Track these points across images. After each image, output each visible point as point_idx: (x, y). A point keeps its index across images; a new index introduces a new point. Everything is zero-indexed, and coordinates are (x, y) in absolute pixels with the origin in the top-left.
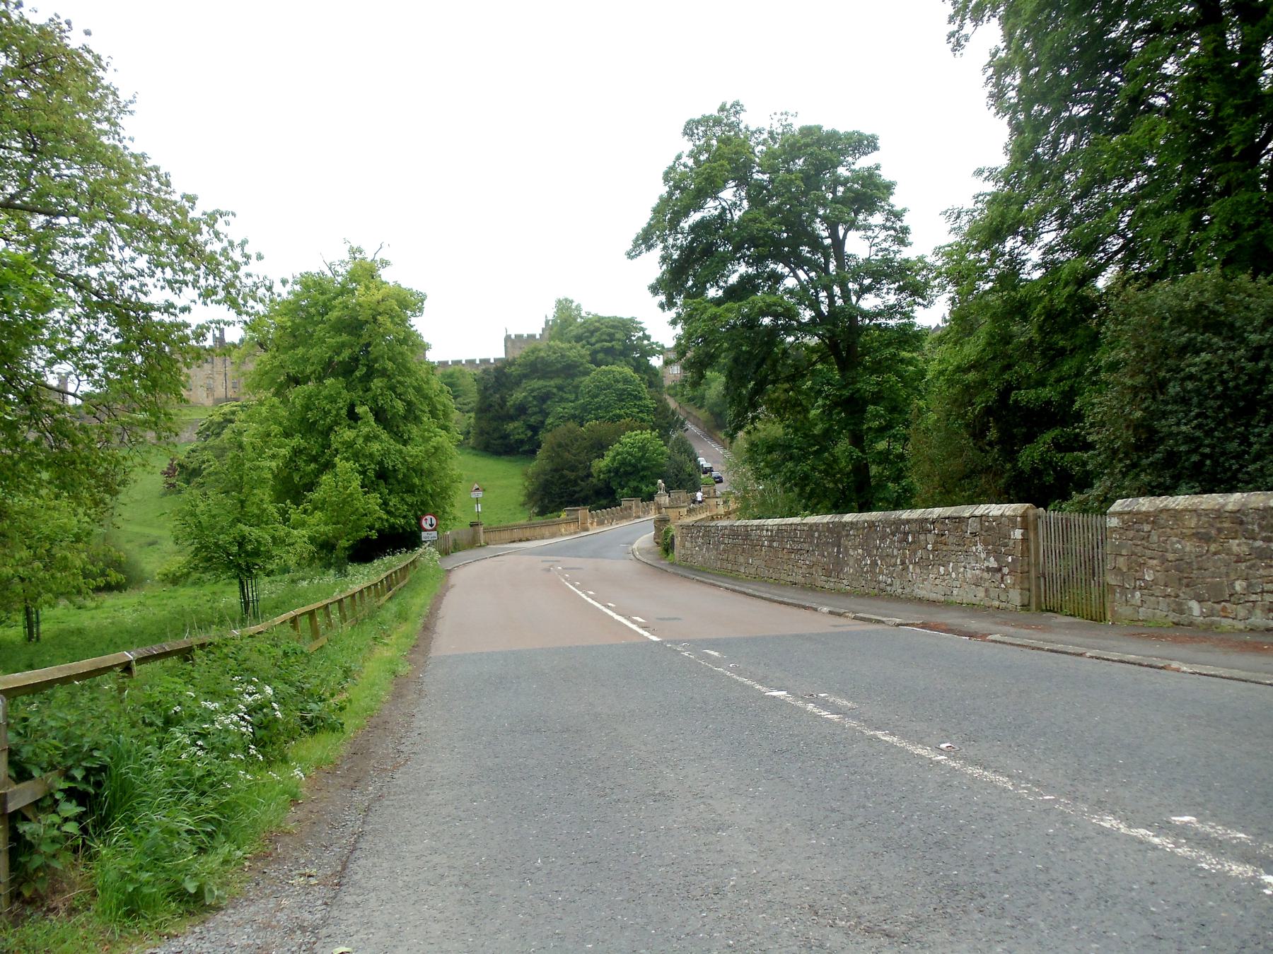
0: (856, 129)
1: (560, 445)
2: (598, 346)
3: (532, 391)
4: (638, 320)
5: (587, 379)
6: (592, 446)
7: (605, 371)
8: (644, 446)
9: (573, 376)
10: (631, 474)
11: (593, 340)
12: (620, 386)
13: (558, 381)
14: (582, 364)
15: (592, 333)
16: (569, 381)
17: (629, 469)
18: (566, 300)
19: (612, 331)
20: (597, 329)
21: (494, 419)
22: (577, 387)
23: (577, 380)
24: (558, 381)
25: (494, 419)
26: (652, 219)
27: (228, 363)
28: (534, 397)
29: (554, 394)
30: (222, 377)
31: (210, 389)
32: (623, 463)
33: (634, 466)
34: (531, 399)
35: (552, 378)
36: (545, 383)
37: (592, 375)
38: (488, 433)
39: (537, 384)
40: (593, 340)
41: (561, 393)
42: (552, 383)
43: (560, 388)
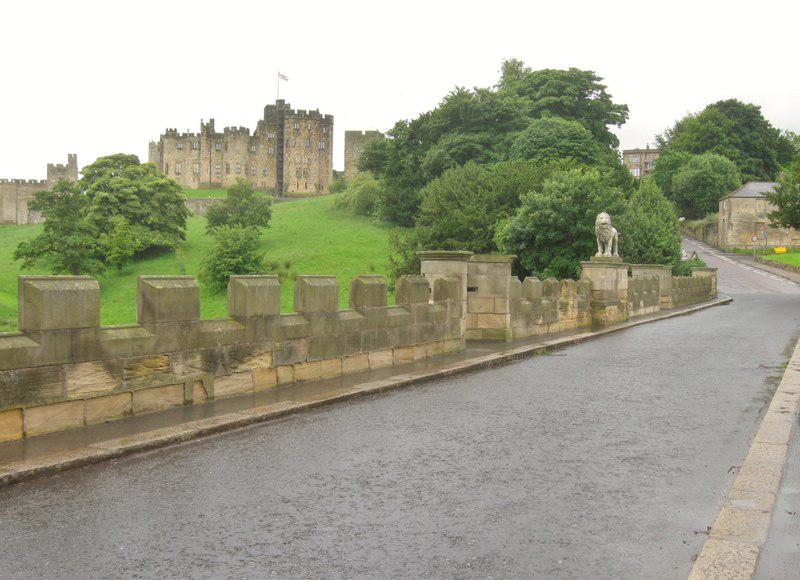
0: (714, 99)
1: (450, 197)
2: (543, 101)
3: (451, 146)
4: (597, 75)
5: (522, 134)
6: (501, 201)
7: (546, 123)
8: (584, 196)
9: (504, 130)
10: (558, 243)
11: (538, 94)
12: (564, 142)
13: (486, 136)
14: (517, 115)
15: (537, 87)
16: (500, 136)
17: (552, 235)
18: (514, 61)
19: (563, 83)
20: (545, 81)
21: (404, 185)
22: (509, 144)
23: (510, 135)
24: (486, 136)
25: (404, 185)
26: (605, 98)
27: (213, 150)
28: (452, 155)
29: (478, 152)
30: (208, 163)
31: (197, 175)
32: (541, 225)
33: (564, 230)
34: (448, 157)
35: (477, 132)
36: (467, 137)
37: (529, 128)
38: (395, 203)
39: (456, 137)
40: (538, 94)
41: (487, 151)
42: (477, 137)
43: (487, 145)
